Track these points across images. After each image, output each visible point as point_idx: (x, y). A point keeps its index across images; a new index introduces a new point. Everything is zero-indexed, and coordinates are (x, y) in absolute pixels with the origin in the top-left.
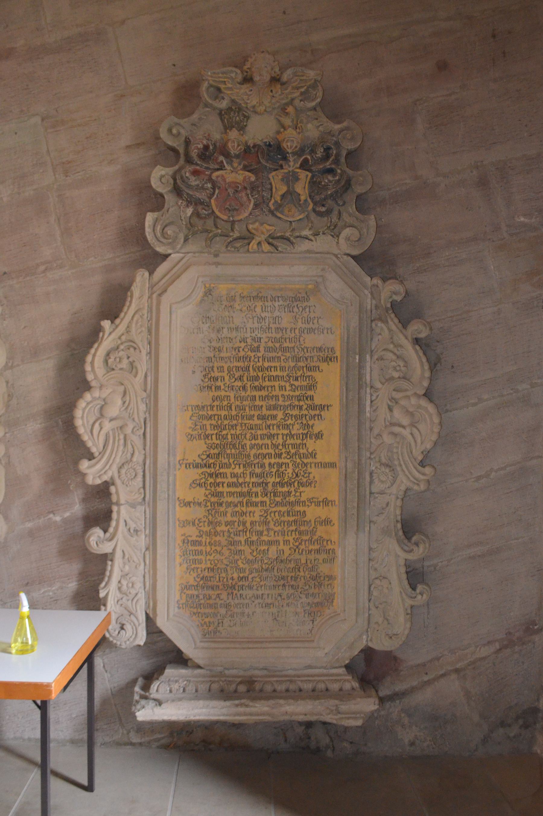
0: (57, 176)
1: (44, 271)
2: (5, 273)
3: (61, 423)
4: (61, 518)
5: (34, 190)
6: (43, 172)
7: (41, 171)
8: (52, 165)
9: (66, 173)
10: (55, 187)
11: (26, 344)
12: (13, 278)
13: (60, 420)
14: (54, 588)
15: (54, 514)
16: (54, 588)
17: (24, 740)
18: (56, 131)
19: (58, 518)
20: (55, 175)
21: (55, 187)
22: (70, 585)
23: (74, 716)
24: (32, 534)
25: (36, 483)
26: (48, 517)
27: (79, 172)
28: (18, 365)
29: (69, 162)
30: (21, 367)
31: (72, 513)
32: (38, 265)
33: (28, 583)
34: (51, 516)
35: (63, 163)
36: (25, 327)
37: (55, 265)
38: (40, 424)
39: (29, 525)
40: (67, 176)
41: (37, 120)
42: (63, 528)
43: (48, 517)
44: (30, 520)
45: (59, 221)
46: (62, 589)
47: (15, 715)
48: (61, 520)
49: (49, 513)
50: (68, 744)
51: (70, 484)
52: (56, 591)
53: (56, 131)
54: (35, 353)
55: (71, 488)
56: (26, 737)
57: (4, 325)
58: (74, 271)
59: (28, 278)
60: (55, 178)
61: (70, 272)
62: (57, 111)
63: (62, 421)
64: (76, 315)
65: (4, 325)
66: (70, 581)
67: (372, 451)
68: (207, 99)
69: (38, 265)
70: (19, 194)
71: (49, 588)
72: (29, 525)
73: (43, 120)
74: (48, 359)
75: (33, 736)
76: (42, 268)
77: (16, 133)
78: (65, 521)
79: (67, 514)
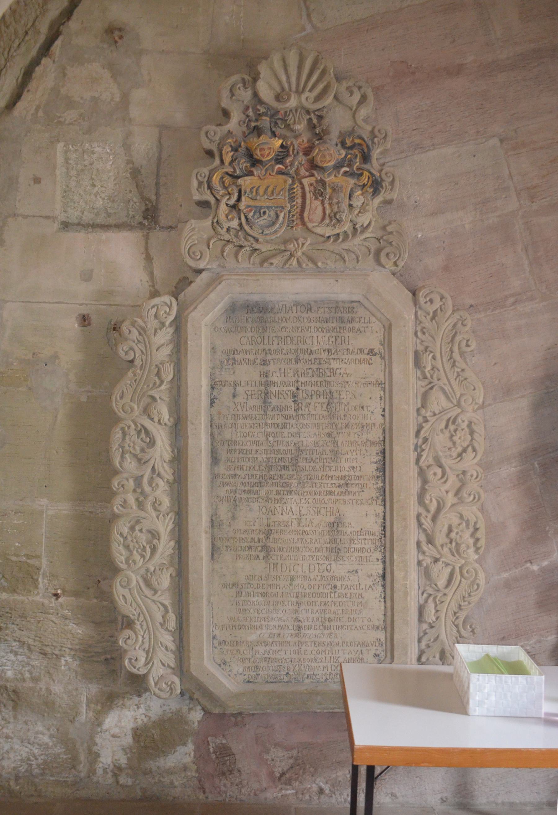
0: (522, 202)
1: (514, 303)
2: (471, 306)
3: (537, 466)
4: (539, 567)
5: (499, 216)
6: (506, 197)
7: (504, 196)
8: (516, 190)
9: (532, 198)
10: (520, 213)
11: (497, 382)
12: (480, 312)
13: (536, 463)
14: (531, 642)
15: (531, 563)
16: (531, 642)
17: (497, 804)
18: (517, 154)
19: (535, 568)
20: (519, 201)
21: (520, 213)
22: (549, 638)
23: (551, 777)
24: (507, 584)
25: (512, 530)
26: (525, 567)
27: (545, 198)
28: (490, 405)
29: (535, 187)
30: (493, 406)
31: (551, 562)
32: (506, 297)
33: (504, 638)
34: (528, 565)
35: (528, 188)
36: (495, 364)
37: (525, 297)
38: (515, 467)
39: (505, 575)
40: (533, 202)
41: (495, 141)
42: (541, 578)
43: (525, 567)
44: (507, 570)
45: (526, 251)
46: (540, 642)
47: (489, 779)
48: (539, 569)
49: (526, 562)
50: (545, 807)
51: (549, 531)
52: (534, 645)
53: (517, 154)
54: (508, 391)
55: (549, 535)
56: (500, 801)
57: (474, 362)
58: (545, 303)
59: (497, 311)
60: (520, 204)
61: (541, 304)
62: (515, 132)
63: (538, 464)
64: (551, 350)
65: (474, 362)
66: (549, 633)
67: (383, 382)
68: (373, 102)
69: (506, 297)
70: (482, 220)
71: (526, 642)
72: (505, 575)
73: (502, 141)
74: (521, 397)
75: (507, 800)
76: (511, 300)
77: (474, 156)
78: (543, 570)
79: (545, 563)
